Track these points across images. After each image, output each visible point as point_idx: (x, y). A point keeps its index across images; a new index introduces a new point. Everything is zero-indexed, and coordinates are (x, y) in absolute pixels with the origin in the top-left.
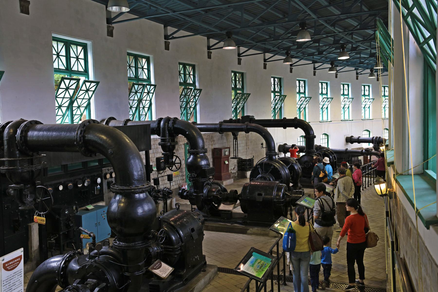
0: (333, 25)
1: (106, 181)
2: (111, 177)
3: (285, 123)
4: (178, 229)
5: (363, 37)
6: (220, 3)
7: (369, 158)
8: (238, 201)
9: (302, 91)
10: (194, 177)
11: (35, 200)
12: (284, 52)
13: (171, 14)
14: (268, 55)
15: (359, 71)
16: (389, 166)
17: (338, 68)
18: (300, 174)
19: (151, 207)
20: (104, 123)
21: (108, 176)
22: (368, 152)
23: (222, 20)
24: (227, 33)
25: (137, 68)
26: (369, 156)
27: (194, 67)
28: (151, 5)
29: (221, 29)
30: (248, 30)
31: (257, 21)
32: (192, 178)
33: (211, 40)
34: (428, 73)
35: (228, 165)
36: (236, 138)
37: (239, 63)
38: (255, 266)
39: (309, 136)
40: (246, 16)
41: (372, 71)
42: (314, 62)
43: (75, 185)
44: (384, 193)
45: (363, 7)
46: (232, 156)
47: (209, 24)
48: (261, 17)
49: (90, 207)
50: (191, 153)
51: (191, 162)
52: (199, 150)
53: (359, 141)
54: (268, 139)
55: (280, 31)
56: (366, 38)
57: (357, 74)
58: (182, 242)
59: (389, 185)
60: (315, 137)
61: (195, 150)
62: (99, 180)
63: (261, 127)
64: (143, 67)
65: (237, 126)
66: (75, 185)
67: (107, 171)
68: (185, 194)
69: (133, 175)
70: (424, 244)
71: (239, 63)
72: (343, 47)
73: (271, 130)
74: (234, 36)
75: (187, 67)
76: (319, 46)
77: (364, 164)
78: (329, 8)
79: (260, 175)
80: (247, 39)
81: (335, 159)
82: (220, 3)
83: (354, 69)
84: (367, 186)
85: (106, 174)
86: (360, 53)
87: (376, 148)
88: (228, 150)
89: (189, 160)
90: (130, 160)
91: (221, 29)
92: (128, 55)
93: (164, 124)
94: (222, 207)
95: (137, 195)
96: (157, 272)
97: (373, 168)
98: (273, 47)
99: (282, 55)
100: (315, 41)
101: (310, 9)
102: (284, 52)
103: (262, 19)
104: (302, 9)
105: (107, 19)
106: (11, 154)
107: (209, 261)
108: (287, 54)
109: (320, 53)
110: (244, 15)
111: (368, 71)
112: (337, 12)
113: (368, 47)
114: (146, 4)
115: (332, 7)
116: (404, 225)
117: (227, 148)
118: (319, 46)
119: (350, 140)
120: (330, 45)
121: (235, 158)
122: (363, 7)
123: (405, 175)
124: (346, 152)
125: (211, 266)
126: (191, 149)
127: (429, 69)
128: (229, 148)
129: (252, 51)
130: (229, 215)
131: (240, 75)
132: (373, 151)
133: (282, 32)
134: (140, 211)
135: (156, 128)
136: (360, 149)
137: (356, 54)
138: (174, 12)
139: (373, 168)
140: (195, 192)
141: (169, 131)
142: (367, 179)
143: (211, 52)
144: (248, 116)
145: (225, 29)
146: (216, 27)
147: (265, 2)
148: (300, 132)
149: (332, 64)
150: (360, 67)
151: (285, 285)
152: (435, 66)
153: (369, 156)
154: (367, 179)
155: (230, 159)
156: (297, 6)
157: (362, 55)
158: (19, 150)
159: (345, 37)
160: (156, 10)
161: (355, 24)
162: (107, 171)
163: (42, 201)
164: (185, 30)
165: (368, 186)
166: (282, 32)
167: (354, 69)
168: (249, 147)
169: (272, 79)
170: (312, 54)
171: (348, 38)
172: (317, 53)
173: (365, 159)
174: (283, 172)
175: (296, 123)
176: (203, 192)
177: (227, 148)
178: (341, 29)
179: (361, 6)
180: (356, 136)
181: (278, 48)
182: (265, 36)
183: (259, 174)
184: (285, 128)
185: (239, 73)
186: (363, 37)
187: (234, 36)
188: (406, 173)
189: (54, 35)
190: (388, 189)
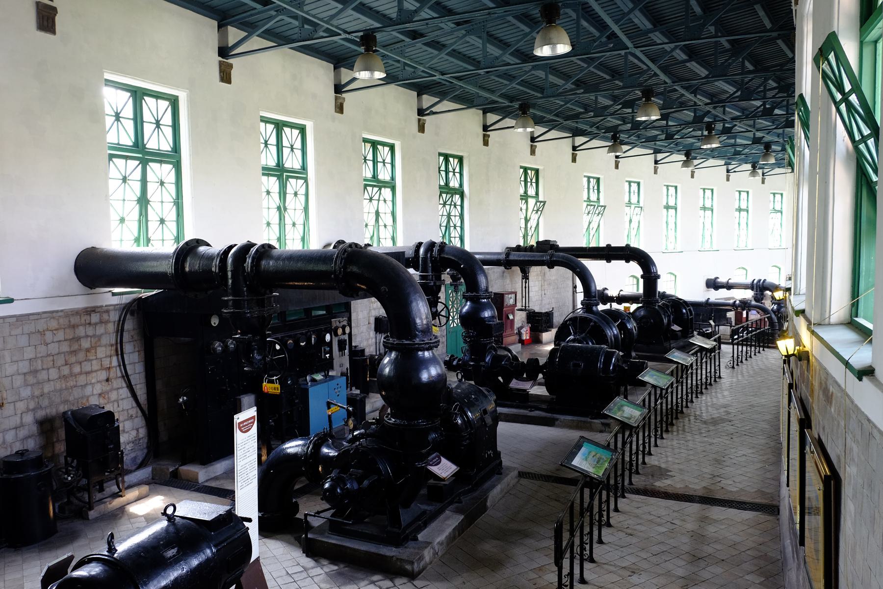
0: (695, 93)
1: (337, 339)
2: (344, 333)
3: (609, 254)
4: (466, 409)
5: (743, 110)
6: (518, 61)
7: (744, 315)
8: (540, 376)
9: (634, 199)
10: (473, 336)
11: (264, 358)
12: (610, 135)
13: (438, 77)
14: (579, 140)
15: (731, 167)
16: (797, 316)
17: (696, 162)
18: (636, 337)
19: (439, 371)
20: (331, 247)
21: (340, 331)
22: (745, 304)
23: (514, 85)
24: (521, 105)
25: (375, 162)
26: (745, 313)
27: (461, 160)
28: (405, 64)
29: (511, 99)
30: (557, 102)
31: (569, 86)
32: (469, 337)
33: (489, 115)
34: (864, 187)
35: (513, 321)
36: (526, 277)
37: (533, 152)
38: (589, 459)
39: (650, 278)
40: (552, 79)
41: (754, 167)
42: (657, 151)
43: (297, 343)
44: (791, 352)
45: (747, 64)
46: (519, 306)
47: (492, 92)
48: (577, 80)
49: (319, 377)
50: (467, 299)
51: (468, 312)
52: (481, 293)
53: (729, 286)
54: (585, 277)
55: (604, 101)
56: (747, 112)
57: (728, 171)
58: (472, 429)
59: (798, 342)
60: (658, 277)
61: (474, 294)
62: (328, 337)
63: (572, 259)
64: (292, 146)
65: (534, 256)
66: (297, 343)
67: (338, 324)
68: (455, 363)
69: (415, 323)
70: (852, 402)
71: (533, 152)
72: (709, 127)
73: (593, 266)
74: (531, 111)
75: (451, 159)
76: (667, 125)
77: (736, 324)
78: (688, 64)
79: (572, 337)
80: (550, 114)
81: (691, 314)
82: (518, 61)
83: (723, 162)
84: (753, 354)
85: (337, 328)
86: (735, 138)
87: (759, 297)
88: (513, 295)
89: (464, 310)
90: (411, 302)
91: (511, 99)
92: (262, 121)
93: (426, 252)
94: (515, 384)
95: (420, 353)
96: (434, 469)
97: (752, 331)
98: (591, 127)
99: (604, 139)
100: (664, 117)
101: (660, 68)
102: (610, 135)
103: (579, 84)
104: (645, 67)
105: (219, 48)
106: (236, 291)
107: (506, 461)
108: (615, 138)
109: (669, 137)
110: (488, 45)
111: (749, 167)
112: (703, 72)
113: (750, 126)
114: (398, 61)
115: (694, 63)
116: (821, 393)
117: (511, 293)
118: (667, 125)
119: (713, 284)
120: (687, 124)
121: (525, 310)
122: (747, 64)
123: (829, 324)
124: (707, 304)
125: (509, 469)
126: (467, 292)
127: (864, 178)
128: (516, 293)
129: (554, 134)
130: (523, 399)
131: (533, 172)
132: (754, 303)
133: (608, 102)
134: (424, 376)
135: (413, 258)
136: (729, 299)
137: (728, 138)
138: (443, 74)
139: (752, 331)
140: (472, 360)
141: (432, 262)
142: (745, 348)
143: (489, 136)
144: (547, 242)
145: (518, 100)
146: (503, 96)
147: (526, 17)
148: (635, 268)
149: (687, 155)
150: (733, 159)
151: (624, 497)
152: (874, 178)
153: (745, 313)
154: (745, 348)
155: (517, 312)
156: (636, 61)
157: (739, 141)
158: (247, 286)
159: (713, 112)
160: (414, 72)
161: (731, 89)
162: (338, 324)
163: (272, 360)
164: (450, 100)
165: (715, 381)
166: (608, 102)
167: (723, 162)
168: (551, 292)
169: (586, 179)
170: (654, 139)
171: (718, 112)
172: (663, 137)
173: (738, 317)
174: (609, 333)
175: (628, 254)
176: (484, 361)
177: (511, 293)
178: (706, 97)
179: (743, 63)
180: (723, 279)
181: (597, 128)
182: (577, 109)
183: (570, 334)
184: (609, 261)
185: (531, 169)
186: (743, 110)
187: (531, 111)
188: (827, 321)
189: (108, 76)
190: (797, 348)
